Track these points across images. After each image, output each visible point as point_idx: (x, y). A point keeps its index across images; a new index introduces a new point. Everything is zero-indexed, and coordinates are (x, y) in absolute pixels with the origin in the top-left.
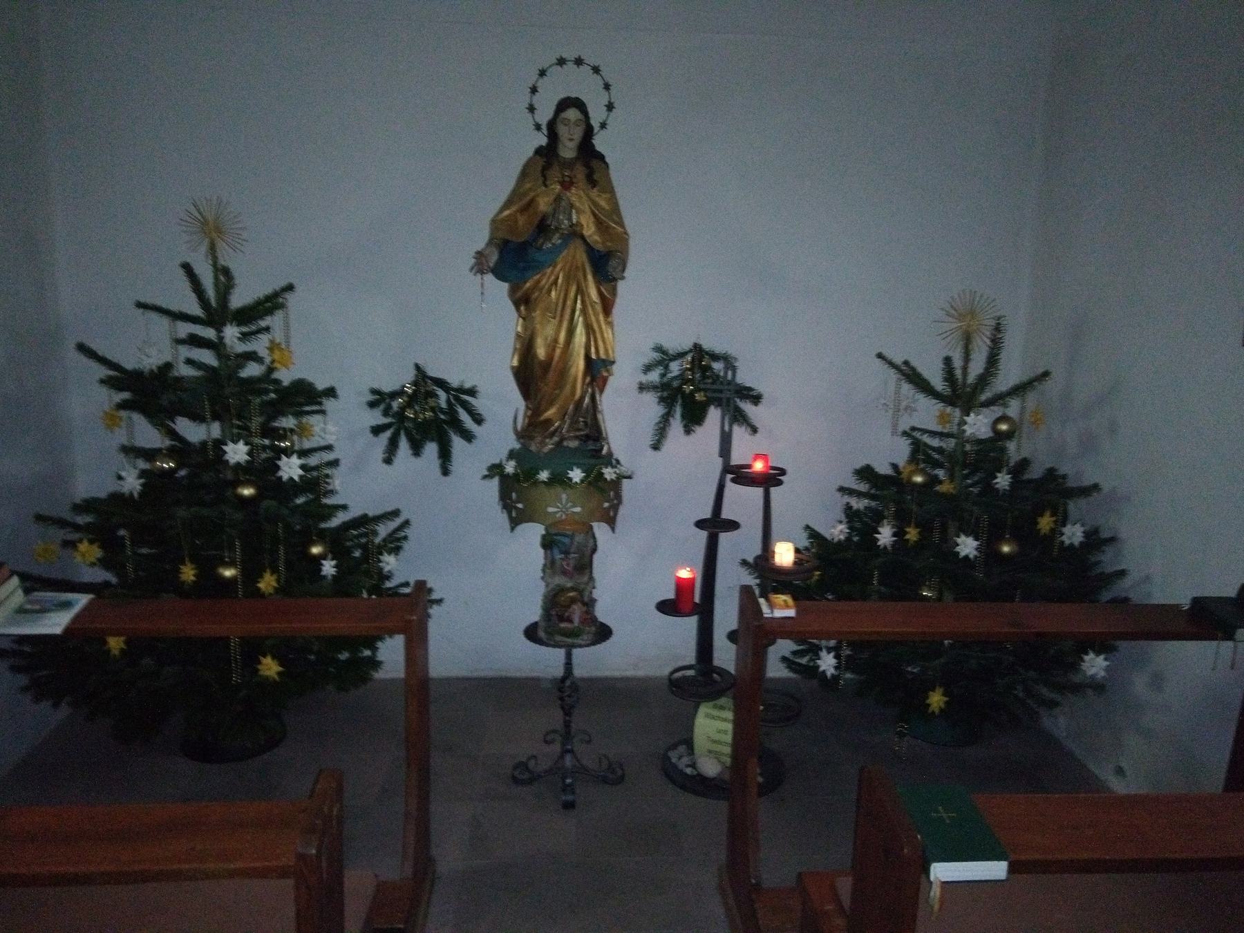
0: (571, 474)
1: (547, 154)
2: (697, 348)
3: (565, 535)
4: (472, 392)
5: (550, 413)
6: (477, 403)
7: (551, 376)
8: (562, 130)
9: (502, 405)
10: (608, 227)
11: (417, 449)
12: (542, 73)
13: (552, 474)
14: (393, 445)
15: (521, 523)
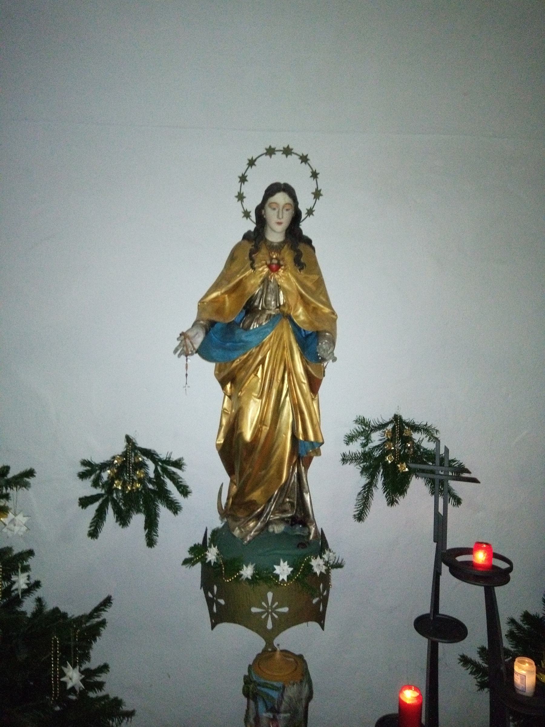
0: (278, 570)
1: (256, 238)
2: (397, 419)
3: (274, 688)
4: (178, 464)
5: (256, 495)
6: (184, 475)
7: (256, 456)
8: (271, 215)
9: (207, 481)
10: (315, 309)
11: (123, 519)
12: (251, 163)
13: (256, 568)
14: (100, 515)
15: (222, 621)
